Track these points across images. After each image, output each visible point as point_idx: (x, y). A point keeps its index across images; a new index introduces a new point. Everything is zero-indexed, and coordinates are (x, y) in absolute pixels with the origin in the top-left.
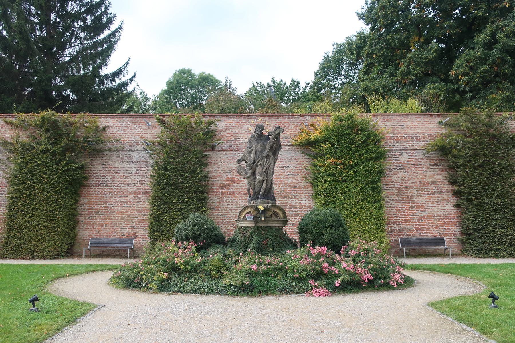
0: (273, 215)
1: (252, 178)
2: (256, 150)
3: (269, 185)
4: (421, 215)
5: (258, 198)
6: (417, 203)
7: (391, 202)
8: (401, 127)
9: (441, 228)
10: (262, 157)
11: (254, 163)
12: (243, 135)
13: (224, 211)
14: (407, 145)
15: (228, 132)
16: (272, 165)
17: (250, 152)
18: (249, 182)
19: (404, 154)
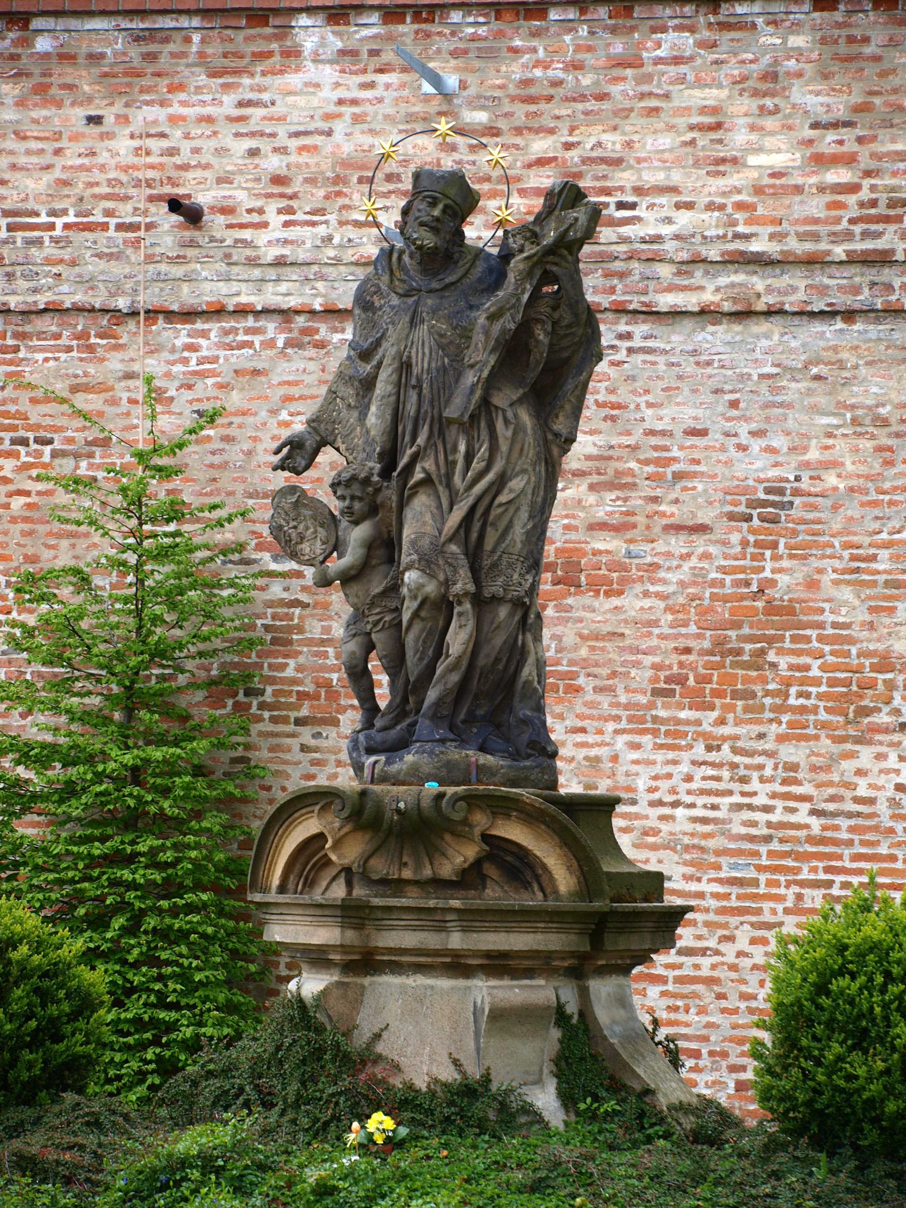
0: (490, 870)
2: (405, 366)
10: (441, 426)
15: (540, 146)
17: (368, 385)
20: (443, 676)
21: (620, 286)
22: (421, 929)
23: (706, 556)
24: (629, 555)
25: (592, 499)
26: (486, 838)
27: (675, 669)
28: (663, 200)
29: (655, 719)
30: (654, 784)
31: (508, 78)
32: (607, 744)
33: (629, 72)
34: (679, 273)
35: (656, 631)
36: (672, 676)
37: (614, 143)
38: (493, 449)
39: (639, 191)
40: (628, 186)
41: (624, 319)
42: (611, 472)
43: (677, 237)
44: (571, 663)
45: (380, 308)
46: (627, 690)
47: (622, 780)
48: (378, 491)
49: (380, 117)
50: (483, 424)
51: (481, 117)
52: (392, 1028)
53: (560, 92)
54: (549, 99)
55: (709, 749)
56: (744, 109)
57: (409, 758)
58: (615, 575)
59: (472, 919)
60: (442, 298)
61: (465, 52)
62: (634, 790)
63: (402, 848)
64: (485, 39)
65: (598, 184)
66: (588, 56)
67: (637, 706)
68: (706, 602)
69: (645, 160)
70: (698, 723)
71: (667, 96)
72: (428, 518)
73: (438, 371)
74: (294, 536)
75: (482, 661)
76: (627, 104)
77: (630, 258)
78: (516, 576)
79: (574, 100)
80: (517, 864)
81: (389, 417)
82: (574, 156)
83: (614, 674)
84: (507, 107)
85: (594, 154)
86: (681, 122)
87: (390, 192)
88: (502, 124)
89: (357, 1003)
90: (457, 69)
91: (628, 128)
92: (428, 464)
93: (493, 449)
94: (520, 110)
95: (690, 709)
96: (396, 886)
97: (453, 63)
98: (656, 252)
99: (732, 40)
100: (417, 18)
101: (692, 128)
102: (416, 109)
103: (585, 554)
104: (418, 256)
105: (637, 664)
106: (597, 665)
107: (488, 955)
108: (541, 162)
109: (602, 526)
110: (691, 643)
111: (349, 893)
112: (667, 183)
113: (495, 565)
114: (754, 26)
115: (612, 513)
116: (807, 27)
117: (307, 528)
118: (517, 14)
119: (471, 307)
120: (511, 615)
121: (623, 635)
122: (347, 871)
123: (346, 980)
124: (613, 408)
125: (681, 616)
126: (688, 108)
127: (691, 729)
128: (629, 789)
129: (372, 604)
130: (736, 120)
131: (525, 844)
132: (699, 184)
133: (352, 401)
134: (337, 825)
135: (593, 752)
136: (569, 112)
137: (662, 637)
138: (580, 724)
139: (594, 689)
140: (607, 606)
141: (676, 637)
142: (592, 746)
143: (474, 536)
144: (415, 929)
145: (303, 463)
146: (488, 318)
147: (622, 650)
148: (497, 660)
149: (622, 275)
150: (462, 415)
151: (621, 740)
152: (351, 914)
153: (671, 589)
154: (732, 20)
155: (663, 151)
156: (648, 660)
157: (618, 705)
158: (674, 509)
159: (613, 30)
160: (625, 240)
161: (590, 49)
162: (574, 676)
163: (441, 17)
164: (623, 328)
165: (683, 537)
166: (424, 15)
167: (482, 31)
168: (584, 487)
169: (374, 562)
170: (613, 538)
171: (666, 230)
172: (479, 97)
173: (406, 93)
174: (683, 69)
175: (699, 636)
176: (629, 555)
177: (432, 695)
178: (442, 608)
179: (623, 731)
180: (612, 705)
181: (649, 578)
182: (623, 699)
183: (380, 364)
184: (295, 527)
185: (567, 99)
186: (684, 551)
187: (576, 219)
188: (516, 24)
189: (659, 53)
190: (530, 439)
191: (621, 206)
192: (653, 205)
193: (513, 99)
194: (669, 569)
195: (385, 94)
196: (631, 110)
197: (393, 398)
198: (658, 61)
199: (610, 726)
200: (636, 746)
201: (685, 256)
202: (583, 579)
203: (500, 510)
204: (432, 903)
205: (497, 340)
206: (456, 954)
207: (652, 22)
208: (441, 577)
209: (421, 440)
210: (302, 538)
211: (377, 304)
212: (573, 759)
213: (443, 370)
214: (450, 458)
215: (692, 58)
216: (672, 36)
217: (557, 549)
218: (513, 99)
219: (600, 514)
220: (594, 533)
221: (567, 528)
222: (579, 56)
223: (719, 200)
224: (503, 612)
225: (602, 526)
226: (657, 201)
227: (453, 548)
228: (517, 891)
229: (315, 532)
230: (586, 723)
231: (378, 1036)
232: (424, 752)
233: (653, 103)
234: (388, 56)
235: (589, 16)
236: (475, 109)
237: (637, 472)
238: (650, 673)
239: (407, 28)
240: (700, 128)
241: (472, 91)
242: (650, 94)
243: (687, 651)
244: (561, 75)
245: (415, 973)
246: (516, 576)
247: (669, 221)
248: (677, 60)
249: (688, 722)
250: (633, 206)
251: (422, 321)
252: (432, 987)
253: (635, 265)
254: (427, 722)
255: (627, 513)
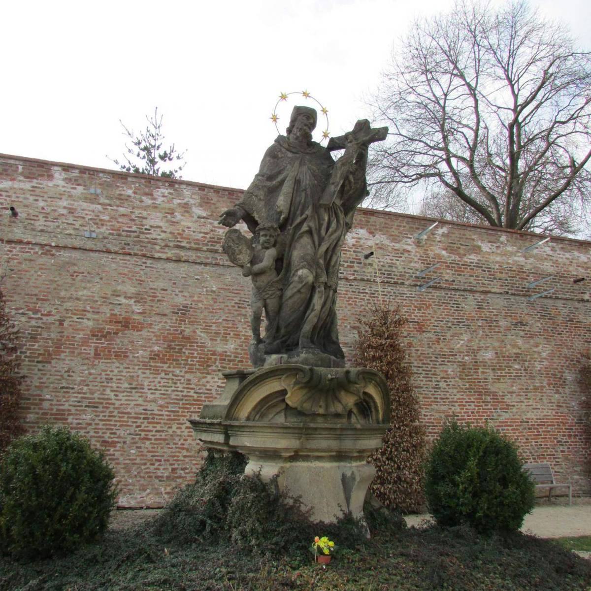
2: (297, 182)
4: (502, 419)
6: (495, 394)
7: (451, 391)
8: (464, 247)
9: (533, 444)
10: (316, 208)
13: (96, 395)
14: (474, 282)
19: (470, 297)
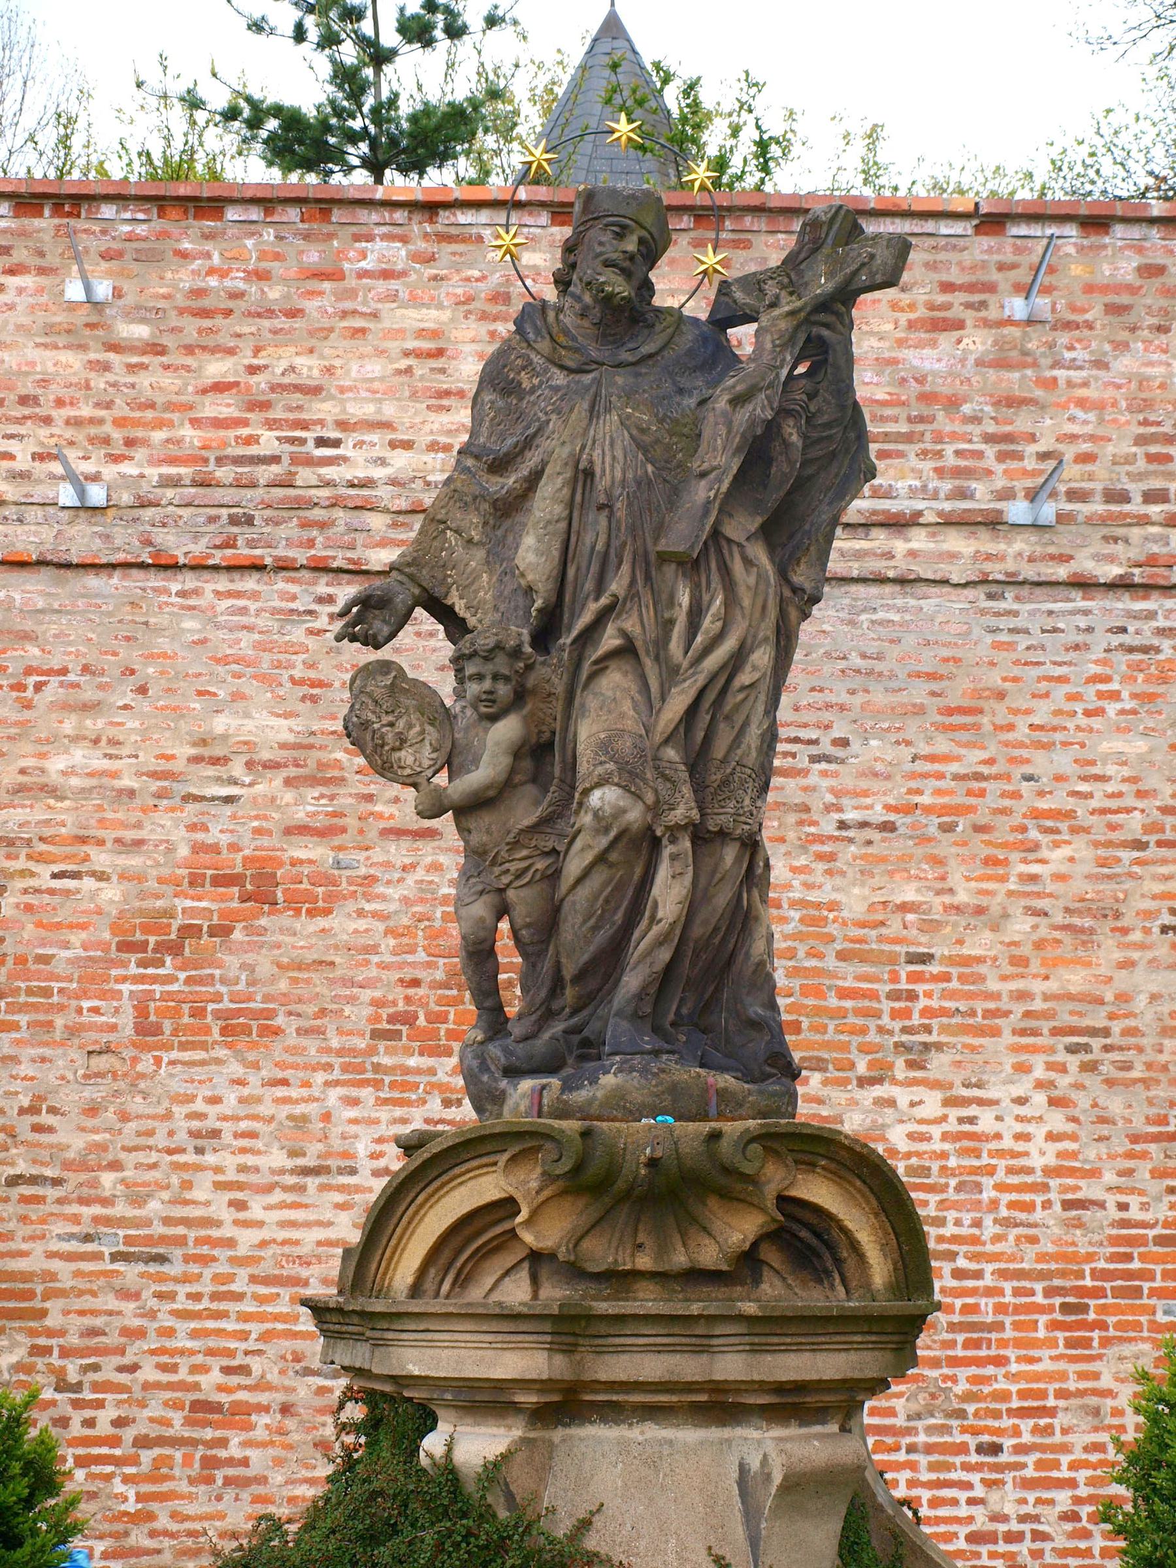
0: (771, 1255)
1: (524, 812)
2: (584, 476)
3: (722, 898)
5: (584, 1051)
10: (650, 565)
11: (546, 632)
12: (368, 410)
15: (217, 368)
16: (762, 657)
17: (509, 509)
18: (478, 859)
20: (649, 952)
21: (320, 539)
22: (671, 1349)
23: (436, 867)
24: (338, 864)
25: (289, 796)
26: (783, 1200)
27: (401, 1006)
28: (374, 437)
29: (377, 1068)
30: (378, 1148)
31: (175, 287)
32: (317, 1100)
33: (327, 286)
34: (395, 525)
35: (375, 959)
36: (397, 1014)
37: (310, 368)
38: (731, 600)
39: (342, 425)
40: (329, 419)
41: (324, 578)
42: (312, 764)
43: (393, 482)
44: (267, 998)
45: (533, 390)
46: (340, 1032)
47: (337, 1144)
48: (529, 668)
49: (11, 327)
50: (713, 565)
51: (141, 331)
52: (608, 1511)
53: (239, 305)
54: (228, 313)
55: (447, 1103)
56: (470, 334)
57: (609, 1080)
58: (320, 890)
59: (771, 1329)
60: (638, 375)
61: (119, 255)
62: (353, 1156)
63: (638, 1220)
64: (145, 239)
65: (291, 416)
66: (276, 264)
67: (353, 1052)
68: (437, 924)
69: (350, 389)
70: (432, 1071)
71: (375, 315)
72: (627, 706)
73: (639, 484)
74: (390, 738)
75: (697, 931)
76: (325, 323)
77: (333, 505)
78: (747, 802)
79: (259, 315)
80: (814, 1242)
81: (556, 554)
82: (260, 382)
83: (323, 1012)
84: (174, 320)
85: (286, 380)
86: (394, 346)
87: (25, 418)
88: (168, 341)
89: (544, 1470)
90: (109, 274)
91: (327, 351)
92: (630, 624)
93: (731, 600)
94: (191, 327)
95: (421, 1054)
96: (619, 1279)
97: (104, 265)
98: (366, 499)
99: (454, 254)
100: (57, 210)
101: (407, 354)
102: (58, 319)
103: (281, 864)
104: (597, 312)
105: (352, 1000)
106: (300, 1001)
107: (780, 1388)
108: (219, 387)
109: (302, 830)
110: (420, 974)
111: (535, 1296)
112: (378, 418)
113: (725, 782)
114: (480, 239)
115: (315, 814)
116: (544, 243)
117: (410, 726)
118: (186, 212)
119: (681, 391)
120: (738, 860)
121: (332, 963)
122: (536, 1258)
123: (532, 1435)
124: (312, 686)
125: (405, 940)
126: (402, 331)
127: (423, 1079)
128: (346, 1155)
129: (515, 845)
130: (460, 347)
131: (834, 1210)
132: (418, 420)
133: (476, 535)
134: (534, 1185)
135: (299, 1110)
136: (253, 329)
137: (382, 966)
138: (280, 1075)
139: (299, 1031)
140: (312, 928)
141: (400, 966)
142: (297, 1102)
143: (700, 735)
144: (659, 1349)
145: (386, 630)
146: (730, 402)
147: (332, 982)
148: (716, 929)
149: (322, 525)
150: (692, 547)
151: (334, 1094)
152: (568, 1329)
153: (393, 907)
154: (453, 231)
155: (372, 380)
156: (367, 995)
157: (328, 1050)
158: (392, 809)
159: (306, 237)
160: (328, 484)
161: (277, 257)
162: (270, 1014)
163: (89, 211)
164: (322, 589)
165: (406, 843)
166: (67, 208)
167: (141, 229)
168: (278, 782)
169: (518, 778)
170: (317, 844)
171: (378, 473)
172: (138, 308)
173: (44, 299)
174: (394, 284)
175: (429, 965)
176: (338, 864)
177: (632, 981)
178: (646, 844)
179: (337, 1083)
180: (321, 1050)
181: (364, 894)
182: (335, 1043)
183: (535, 477)
184: (391, 725)
185: (250, 314)
186: (407, 861)
187: (872, 257)
188: (183, 223)
189: (363, 264)
190: (771, 591)
191: (321, 442)
192: (363, 442)
193: (181, 312)
194: (389, 882)
195: (18, 300)
196: (331, 330)
197: (563, 525)
198: (363, 274)
199: (320, 1077)
200: (355, 1102)
201: (403, 504)
202: (280, 894)
203: (741, 696)
204: (695, 1309)
205: (743, 436)
206: (717, 1387)
207: (354, 229)
208: (650, 798)
209: (617, 586)
210: (402, 741)
211: (526, 385)
212: (273, 1118)
213: (644, 483)
214: (667, 615)
215: (403, 274)
216: (379, 245)
217: (245, 858)
218: (181, 312)
219: (300, 815)
220: (293, 838)
221: (258, 831)
222: (264, 265)
223: (443, 440)
224: (730, 854)
225: (302, 830)
226: (366, 438)
227: (671, 753)
228: (804, 1283)
229: (423, 732)
230: (287, 1074)
231: (585, 1525)
232: (632, 1069)
233: (359, 323)
234: (21, 255)
235: (276, 218)
236: (132, 321)
237: (346, 764)
238: (369, 1011)
239: (45, 223)
240: (418, 354)
241: (130, 299)
242: (354, 312)
243: (415, 983)
244: (241, 285)
245: (642, 1420)
246: (747, 802)
247: (382, 462)
248: (387, 275)
249: (418, 1071)
250: (336, 443)
251: (608, 410)
252: (670, 1443)
253: (339, 513)
254: (625, 1025)
255: (334, 814)
